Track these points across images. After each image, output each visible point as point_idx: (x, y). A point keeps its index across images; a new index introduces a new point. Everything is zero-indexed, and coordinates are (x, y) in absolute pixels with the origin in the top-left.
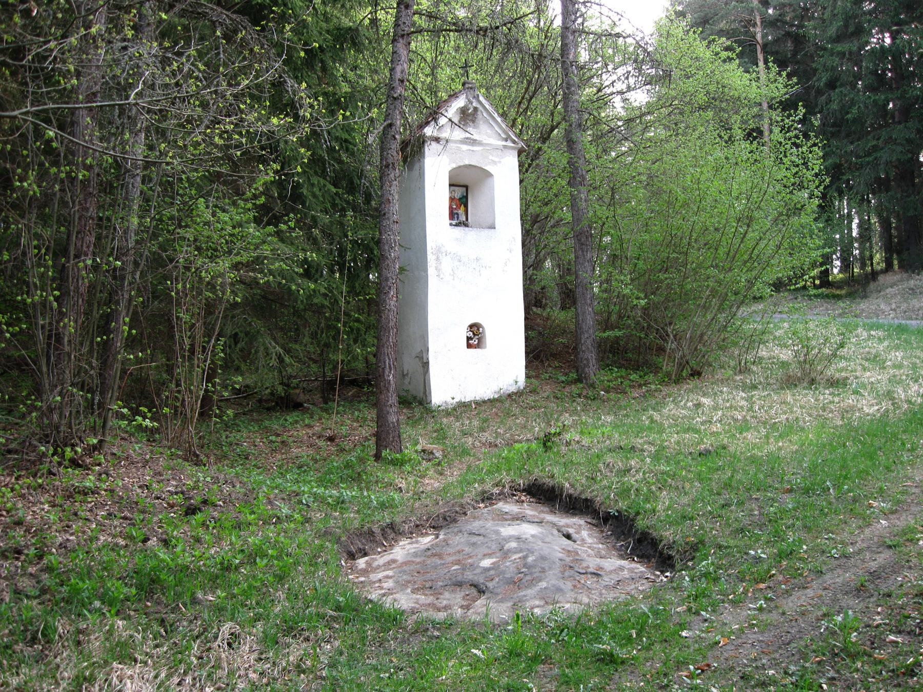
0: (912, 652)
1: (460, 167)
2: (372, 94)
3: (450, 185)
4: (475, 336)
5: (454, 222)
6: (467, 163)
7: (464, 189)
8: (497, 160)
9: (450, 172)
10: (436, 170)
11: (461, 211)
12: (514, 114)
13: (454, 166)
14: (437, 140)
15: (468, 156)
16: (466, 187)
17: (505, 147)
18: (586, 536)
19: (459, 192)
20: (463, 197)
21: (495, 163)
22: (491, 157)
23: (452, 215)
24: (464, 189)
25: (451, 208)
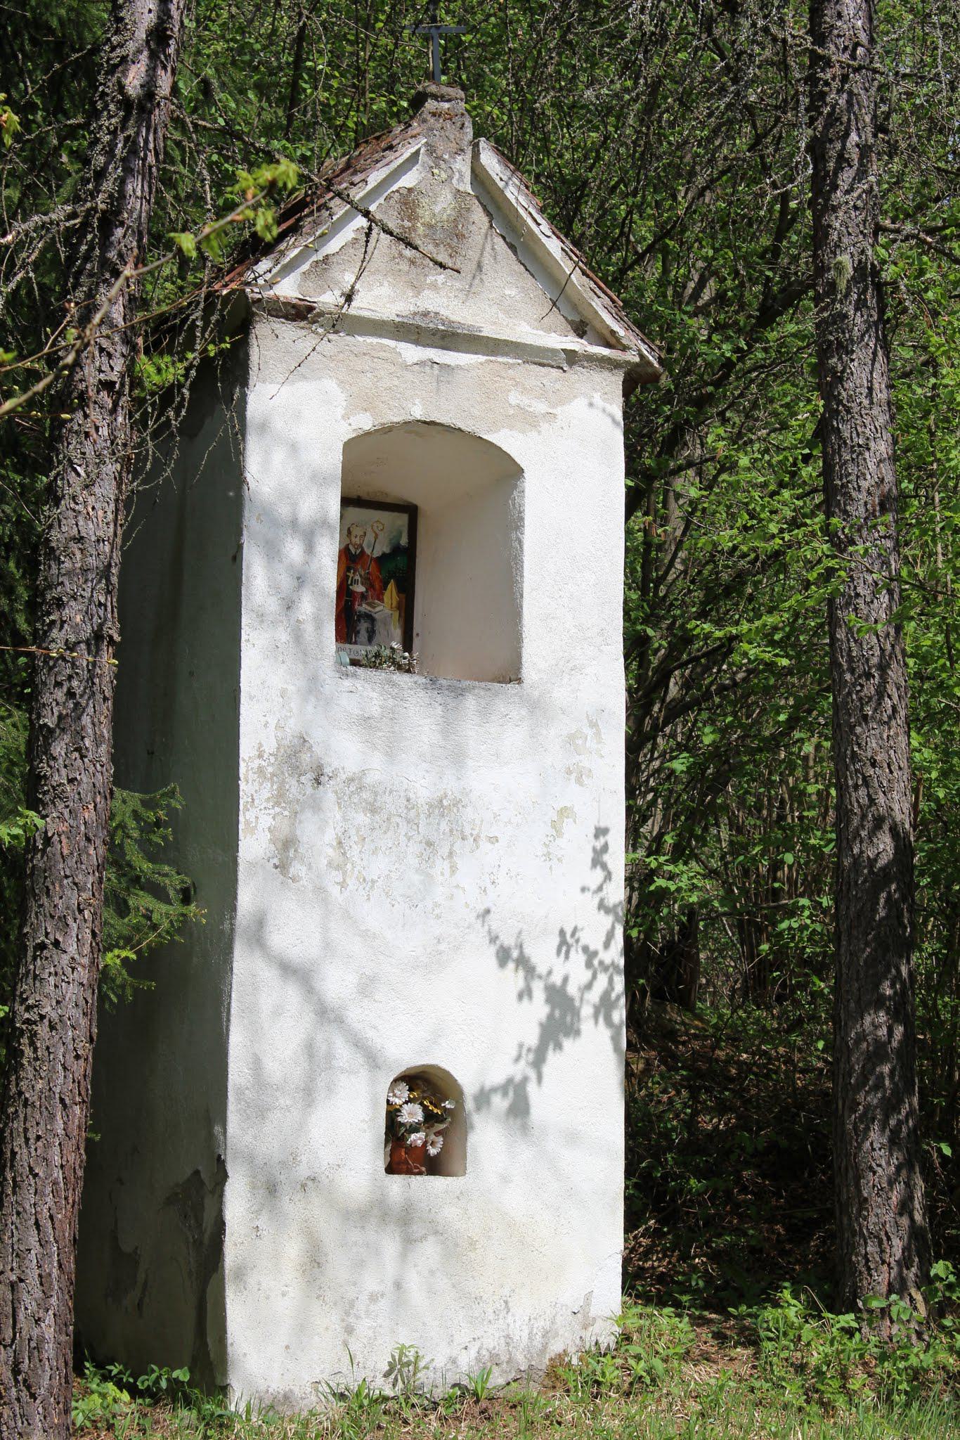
0: (52, 917)
1: (387, 430)
2: (151, 266)
3: (346, 502)
4: (425, 1124)
5: (361, 650)
6: (418, 413)
7: (403, 520)
8: (540, 407)
9: (349, 446)
10: (300, 428)
11: (385, 608)
12: (605, 217)
13: (366, 422)
14: (300, 313)
15: (413, 389)
16: (411, 511)
17: (572, 358)
18: (488, 331)
19: (380, 534)
20: (396, 550)
21: (529, 421)
22: (514, 398)
23: (350, 622)
24: (403, 520)
25: (344, 590)
